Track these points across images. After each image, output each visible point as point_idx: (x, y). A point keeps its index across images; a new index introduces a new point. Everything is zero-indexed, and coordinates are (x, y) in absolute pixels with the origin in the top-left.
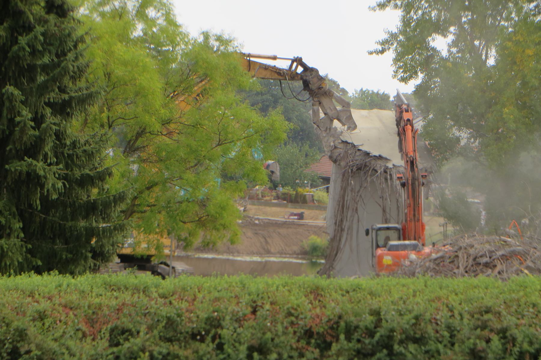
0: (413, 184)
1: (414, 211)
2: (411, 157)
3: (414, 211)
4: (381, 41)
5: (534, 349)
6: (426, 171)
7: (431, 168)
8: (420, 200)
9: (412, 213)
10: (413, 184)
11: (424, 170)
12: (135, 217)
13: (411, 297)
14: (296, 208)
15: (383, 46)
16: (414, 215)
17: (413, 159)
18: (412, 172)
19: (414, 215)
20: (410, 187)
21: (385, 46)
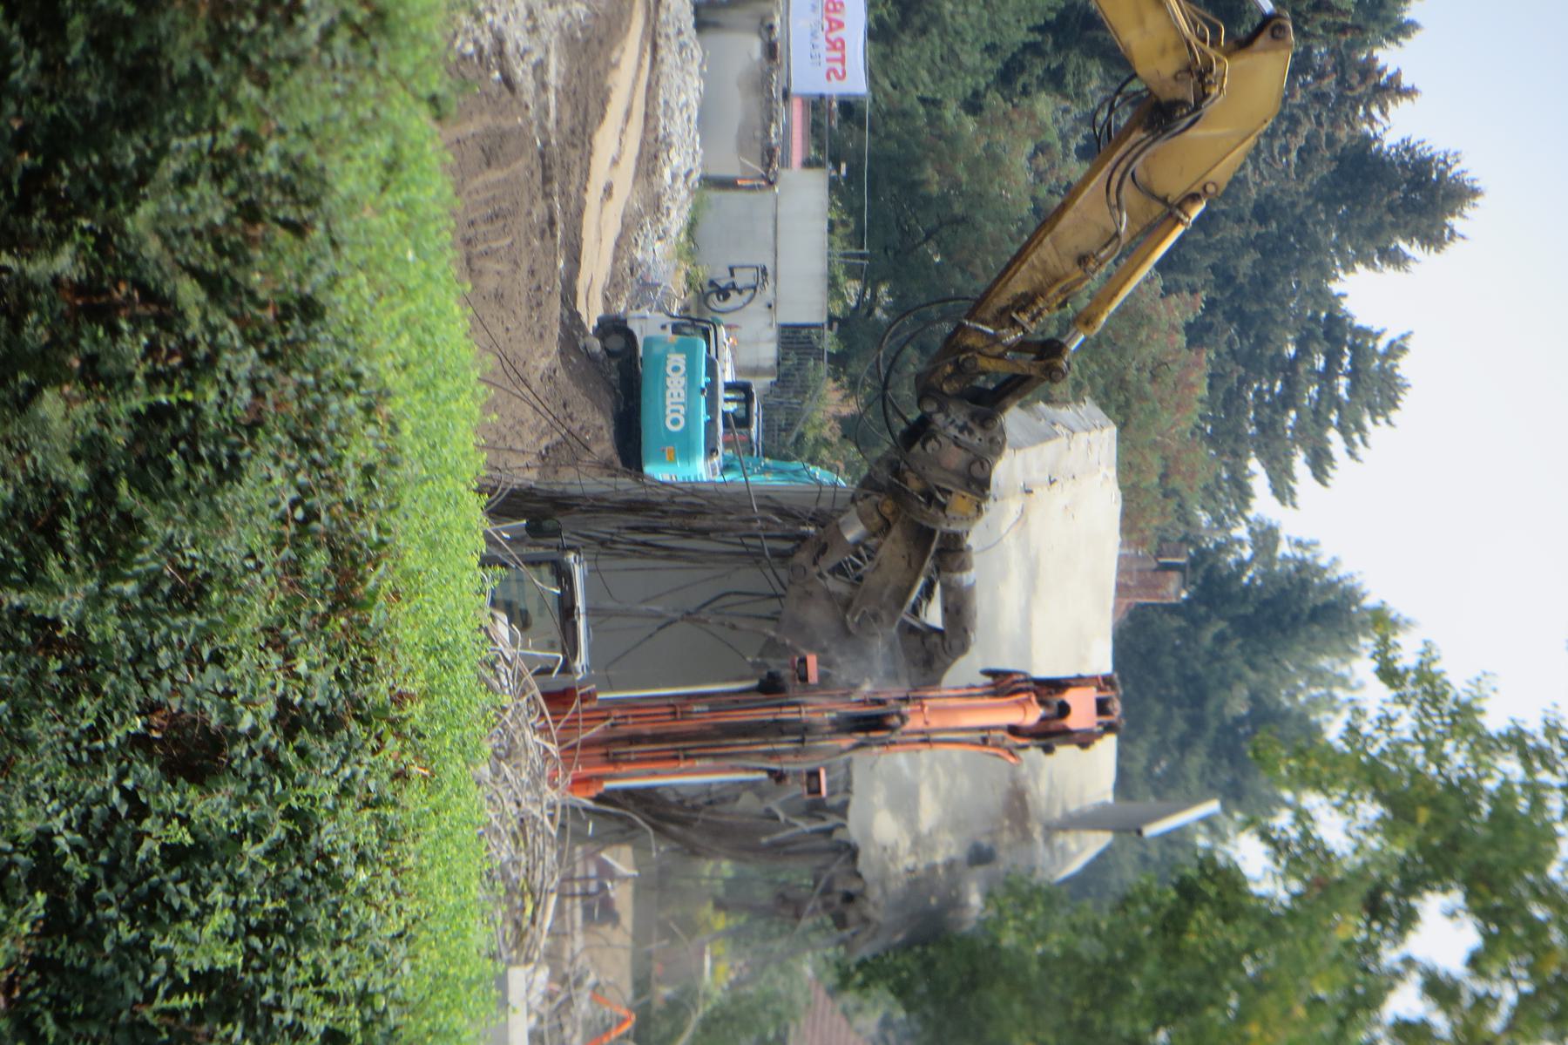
0: (778, 729)
1: (656, 738)
2: (903, 718)
3: (656, 738)
4: (1435, 667)
5: (233, 135)
6: (849, 898)
7: (866, 920)
8: (708, 763)
9: (646, 729)
10: (778, 729)
11: (854, 887)
12: (348, 870)
13: (274, 328)
14: (628, 29)
15: (1412, 676)
16: (634, 739)
17: (892, 729)
18: (833, 722)
19: (634, 739)
20: (766, 715)
21: (1416, 682)
